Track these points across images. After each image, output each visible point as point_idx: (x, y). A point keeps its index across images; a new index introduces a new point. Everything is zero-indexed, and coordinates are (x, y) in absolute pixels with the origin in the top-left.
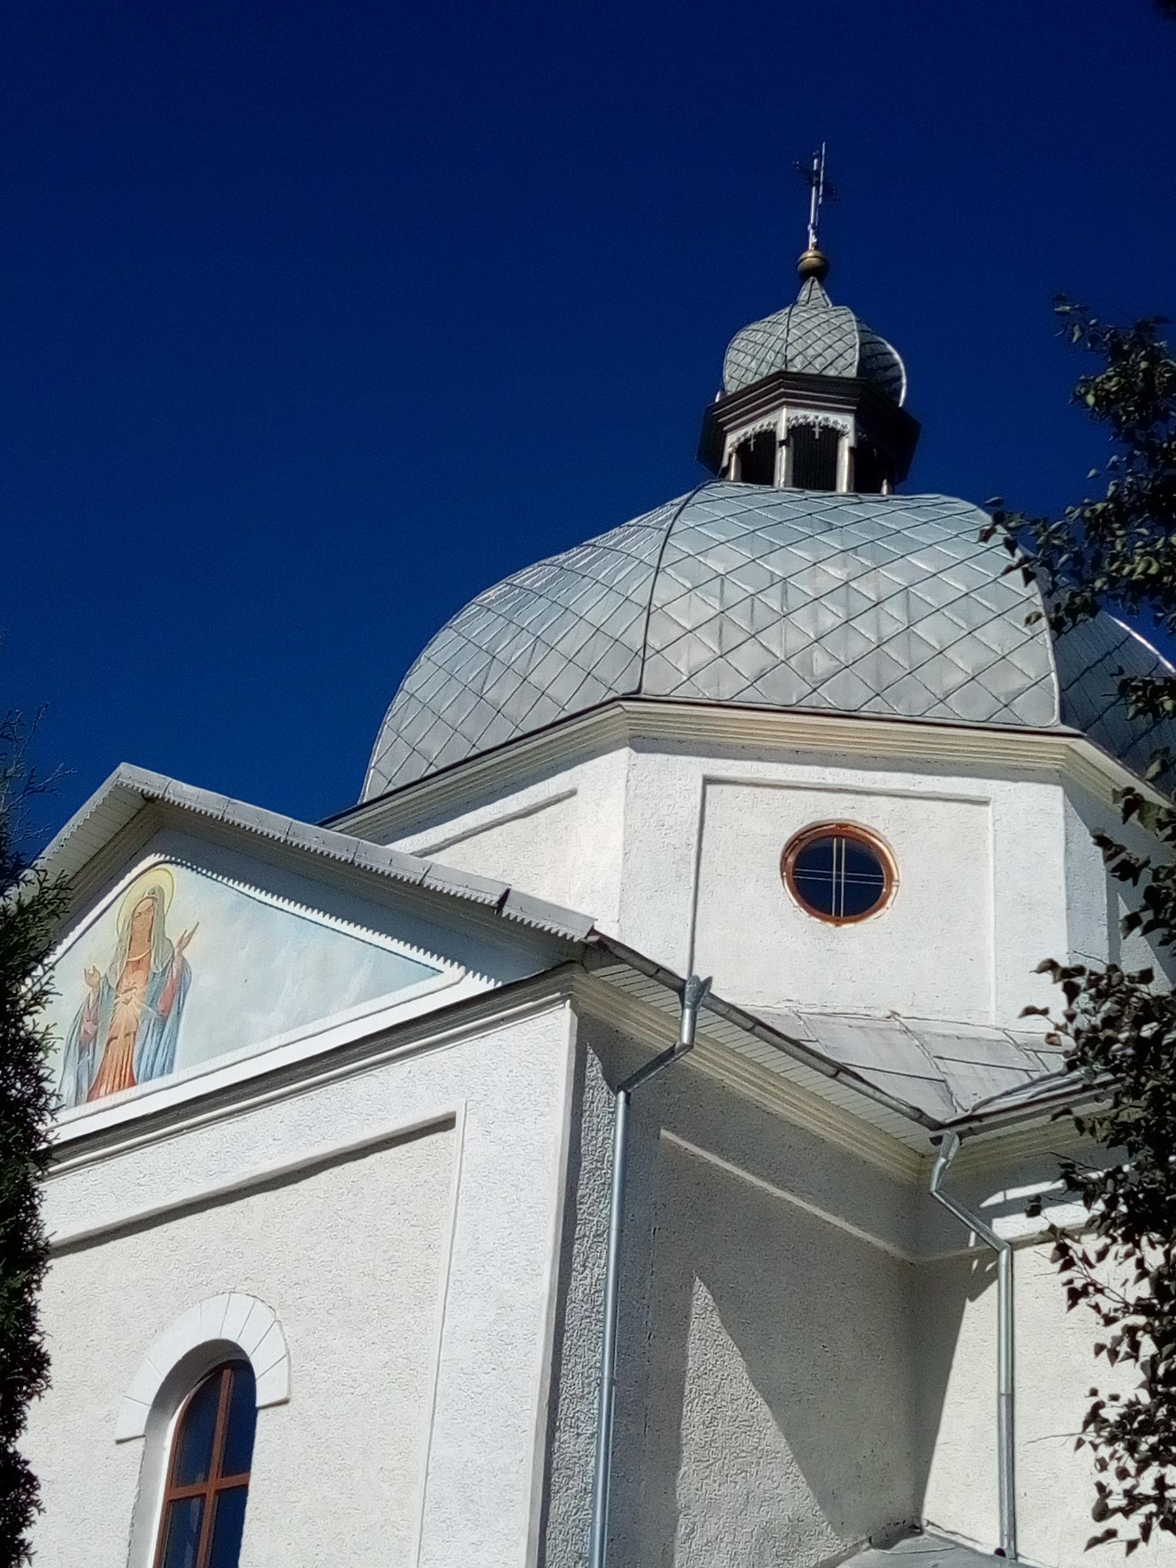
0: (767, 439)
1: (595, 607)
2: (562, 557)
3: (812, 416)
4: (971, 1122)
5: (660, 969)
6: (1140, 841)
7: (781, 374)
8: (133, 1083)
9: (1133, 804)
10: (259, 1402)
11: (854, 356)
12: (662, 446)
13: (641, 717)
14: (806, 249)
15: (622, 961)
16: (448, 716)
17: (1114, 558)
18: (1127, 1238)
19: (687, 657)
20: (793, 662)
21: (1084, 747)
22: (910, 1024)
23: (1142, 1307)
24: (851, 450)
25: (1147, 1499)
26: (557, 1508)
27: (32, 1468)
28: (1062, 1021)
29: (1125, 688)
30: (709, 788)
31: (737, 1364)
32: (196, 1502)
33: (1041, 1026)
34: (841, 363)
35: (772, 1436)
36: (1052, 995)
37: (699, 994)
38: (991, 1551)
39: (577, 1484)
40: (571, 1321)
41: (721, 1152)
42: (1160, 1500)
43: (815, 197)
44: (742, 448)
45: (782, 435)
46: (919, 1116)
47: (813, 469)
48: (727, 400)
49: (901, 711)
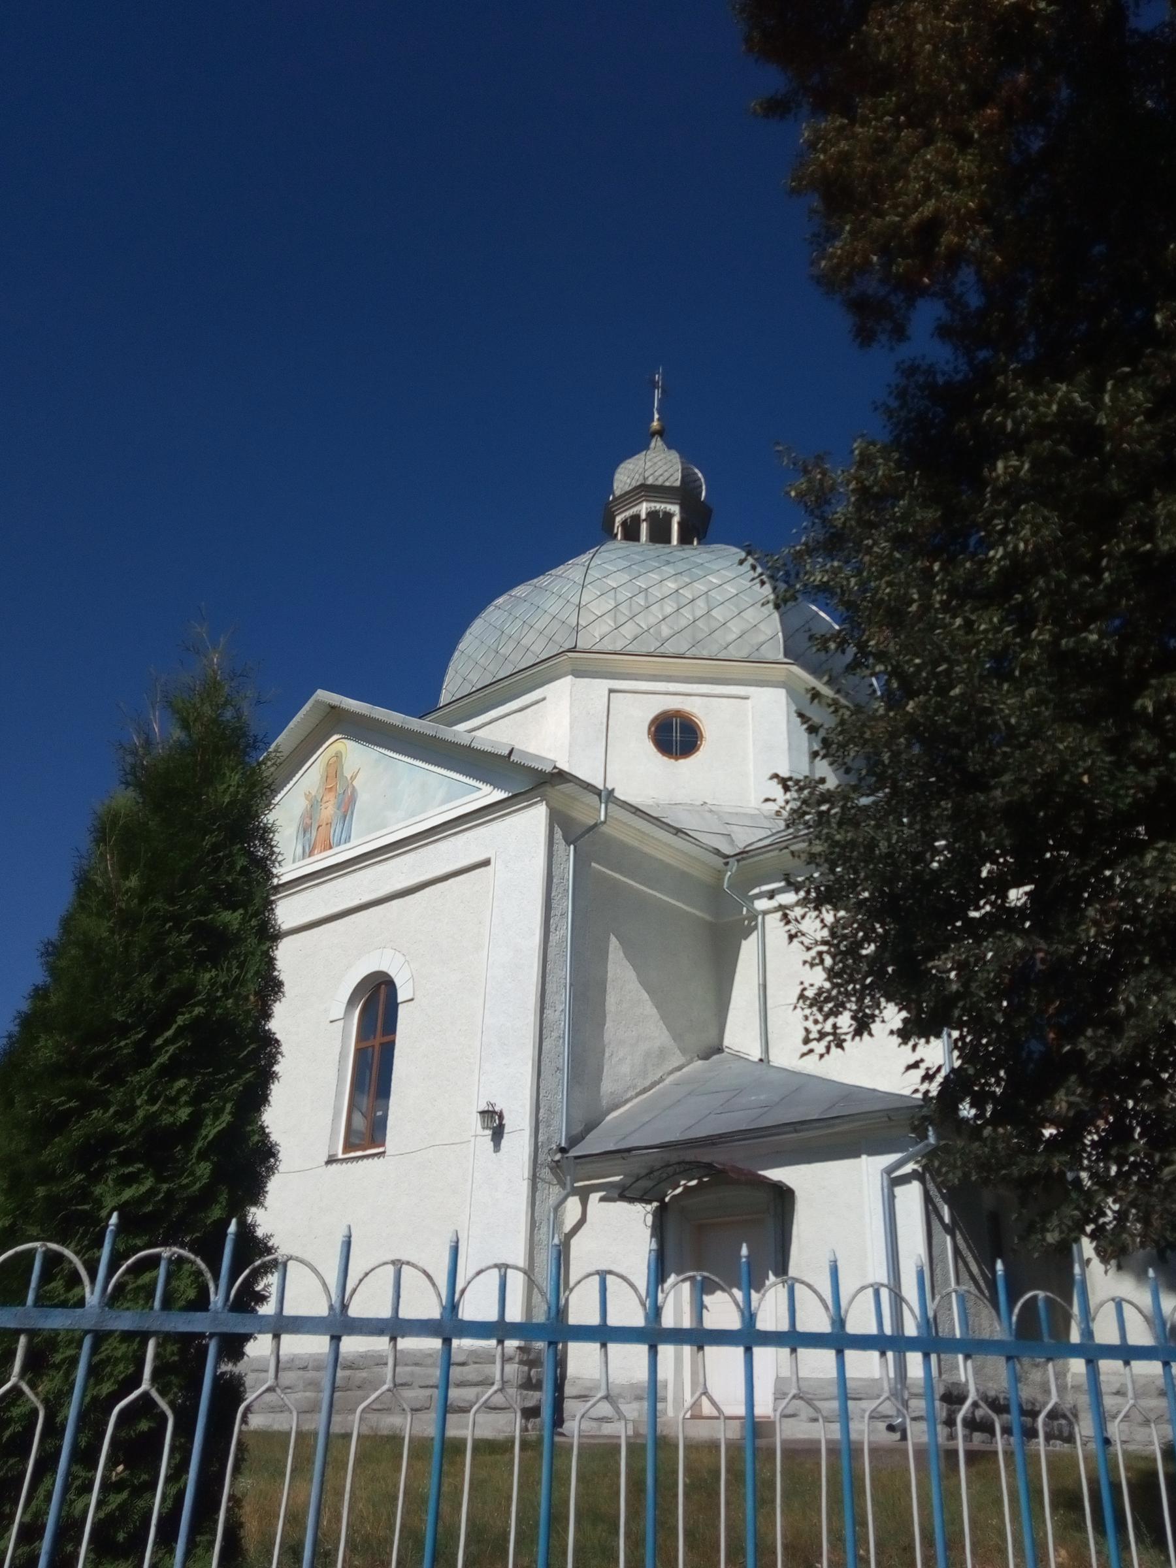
0: (636, 518)
1: (553, 605)
2: (535, 580)
3: (658, 506)
4: (743, 855)
5: (589, 785)
6: (820, 715)
7: (642, 485)
8: (331, 848)
9: (815, 695)
10: (400, 1000)
11: (679, 475)
12: (582, 523)
13: (576, 660)
15: (570, 781)
16: (482, 661)
17: (806, 573)
18: (816, 908)
21: (796, 669)
22: (713, 808)
23: (824, 943)
24: (679, 524)
25: (828, 1034)
26: (547, 1044)
27: (278, 1036)
28: (783, 804)
29: (811, 638)
30: (612, 695)
31: (631, 974)
32: (370, 1049)
33: (774, 807)
34: (672, 479)
35: (649, 1009)
36: (777, 791)
37: (608, 796)
38: (756, 1060)
39: (555, 1034)
40: (550, 956)
41: (621, 873)
42: (834, 1034)
43: (657, 394)
45: (643, 516)
46: (717, 852)
47: (660, 533)
48: (615, 499)
49: (705, 654)
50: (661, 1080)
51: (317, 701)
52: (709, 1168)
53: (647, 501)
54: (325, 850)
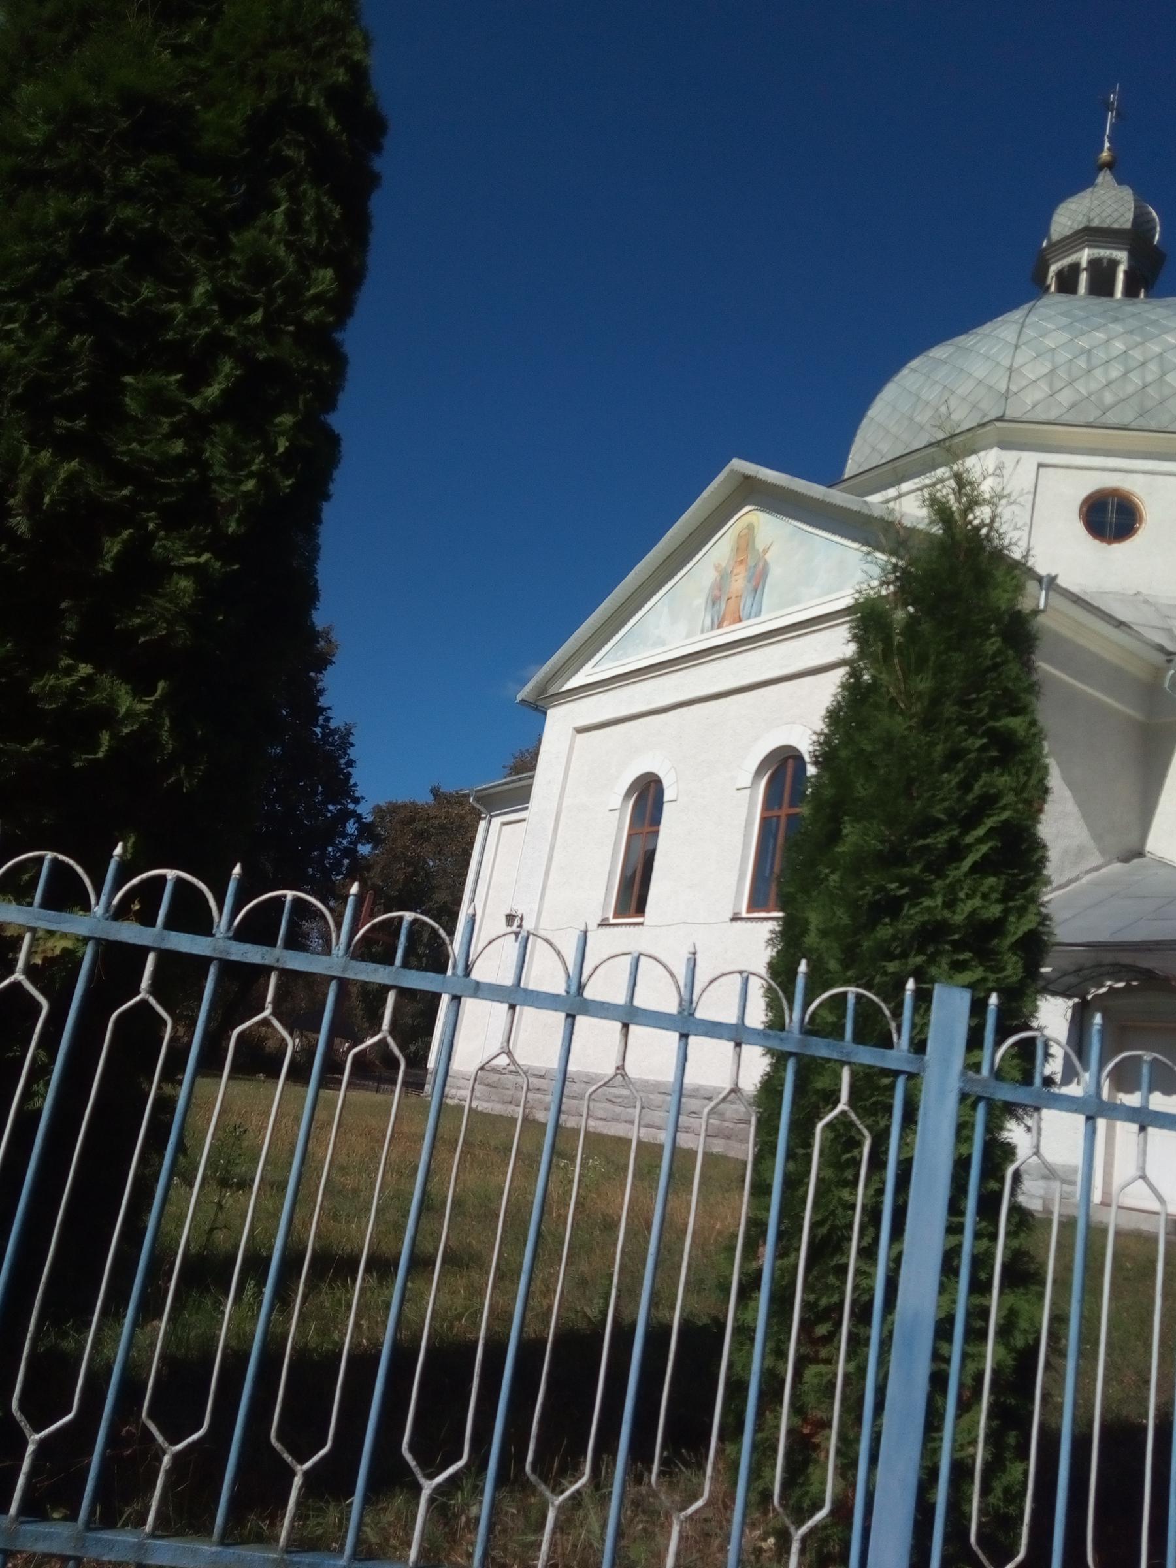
0: (1075, 268)
8: (740, 621)
14: (1102, 150)
19: (1031, 397)
20: (1092, 398)
24: (1126, 273)
30: (1042, 470)
34: (1122, 220)
44: (1060, 274)
45: (1084, 264)
47: (1102, 284)
48: (1051, 245)
49: (1153, 425)
50: (1077, 878)
51: (732, 471)
52: (1147, 976)
53: (1090, 246)
54: (734, 622)
